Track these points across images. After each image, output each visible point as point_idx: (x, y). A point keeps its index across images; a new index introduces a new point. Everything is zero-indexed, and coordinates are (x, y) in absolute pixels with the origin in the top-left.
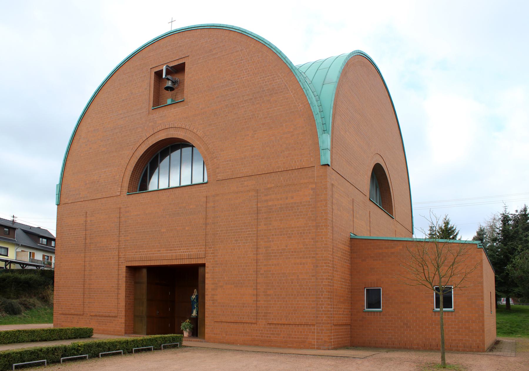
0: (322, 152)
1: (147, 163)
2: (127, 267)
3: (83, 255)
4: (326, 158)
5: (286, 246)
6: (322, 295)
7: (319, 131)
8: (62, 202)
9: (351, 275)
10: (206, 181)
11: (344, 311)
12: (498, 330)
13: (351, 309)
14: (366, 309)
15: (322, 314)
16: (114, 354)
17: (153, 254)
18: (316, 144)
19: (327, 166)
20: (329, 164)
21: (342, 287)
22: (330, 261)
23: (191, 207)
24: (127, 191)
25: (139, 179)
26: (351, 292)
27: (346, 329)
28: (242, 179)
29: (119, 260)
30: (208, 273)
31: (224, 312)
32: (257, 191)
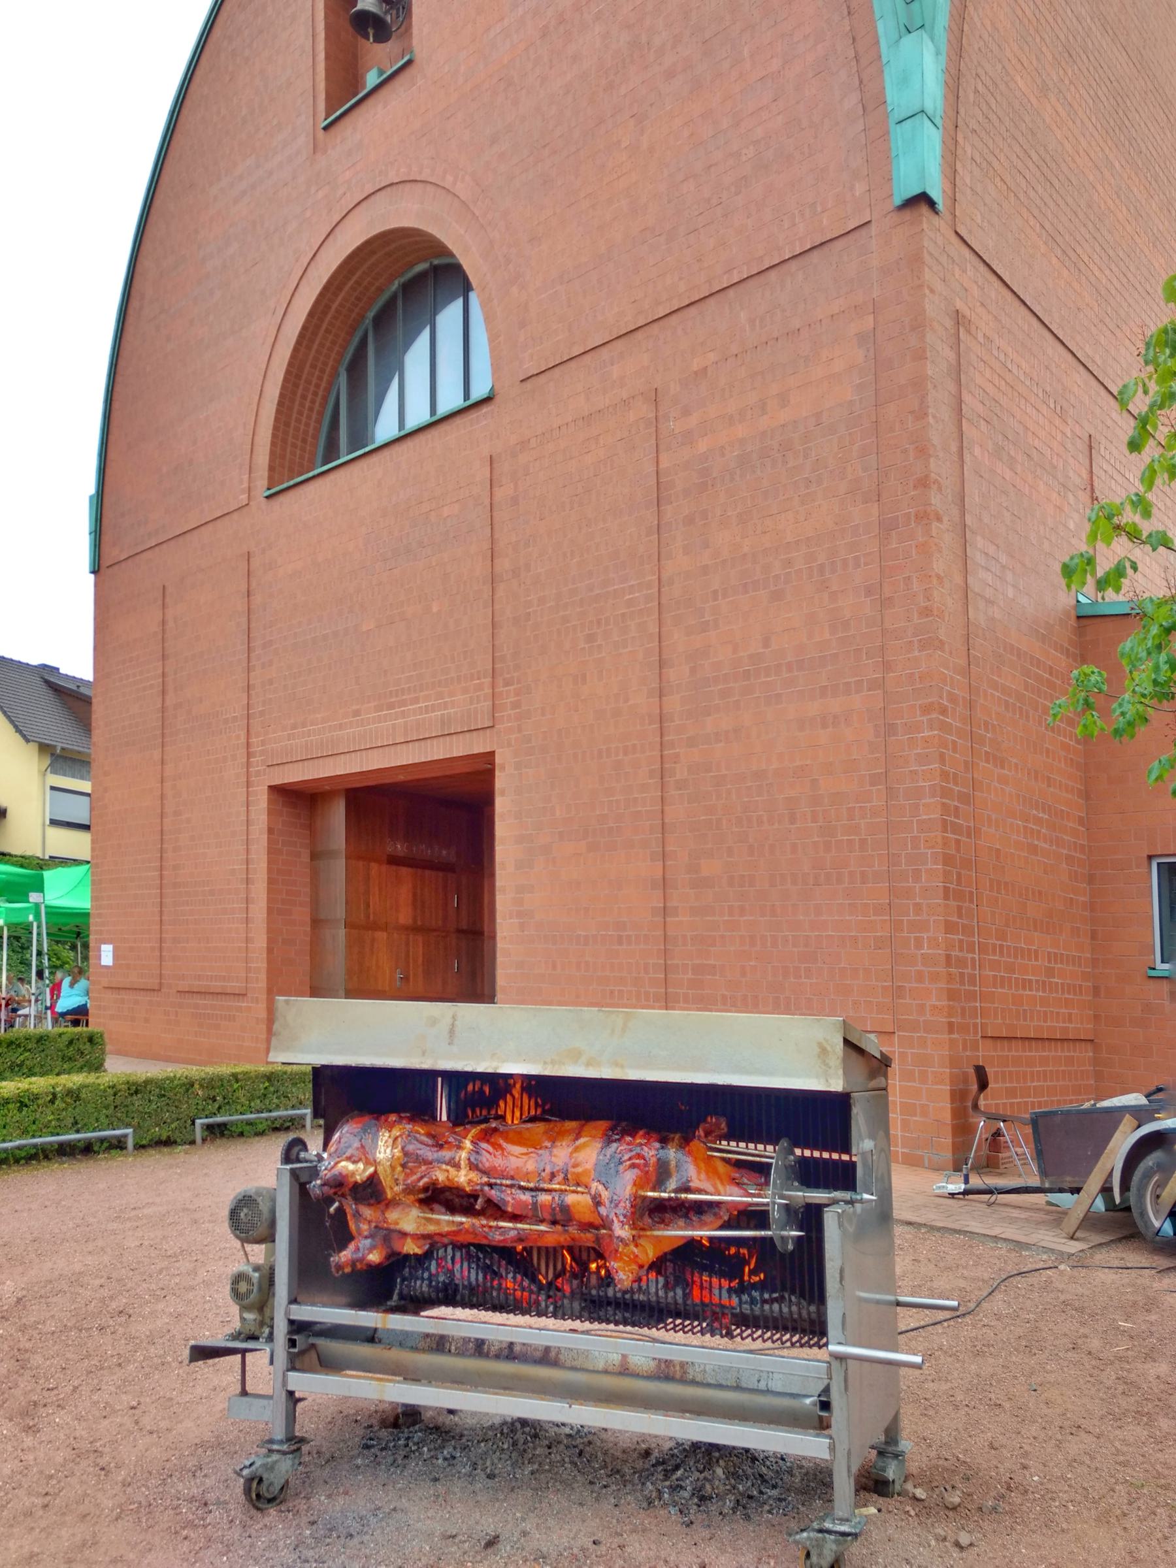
0: (899, 135)
1: (335, 374)
2: (270, 787)
3: (157, 755)
4: (920, 162)
5: (766, 643)
6: (917, 875)
7: (885, 28)
8: (106, 562)
9: (1087, 795)
10: (479, 390)
11: (1050, 972)
12: (551, 1250)
13: (1095, 962)
14: (1160, 966)
15: (920, 977)
16: (65, 1151)
17: (341, 727)
18: (873, 103)
19: (924, 209)
20: (936, 195)
21: (1034, 849)
22: (953, 699)
23: (446, 512)
24: (265, 483)
25: (316, 437)
26: (1091, 879)
27: (1070, 1061)
28: (605, 353)
29: (248, 765)
30: (503, 794)
31: (554, 967)
32: (656, 398)
